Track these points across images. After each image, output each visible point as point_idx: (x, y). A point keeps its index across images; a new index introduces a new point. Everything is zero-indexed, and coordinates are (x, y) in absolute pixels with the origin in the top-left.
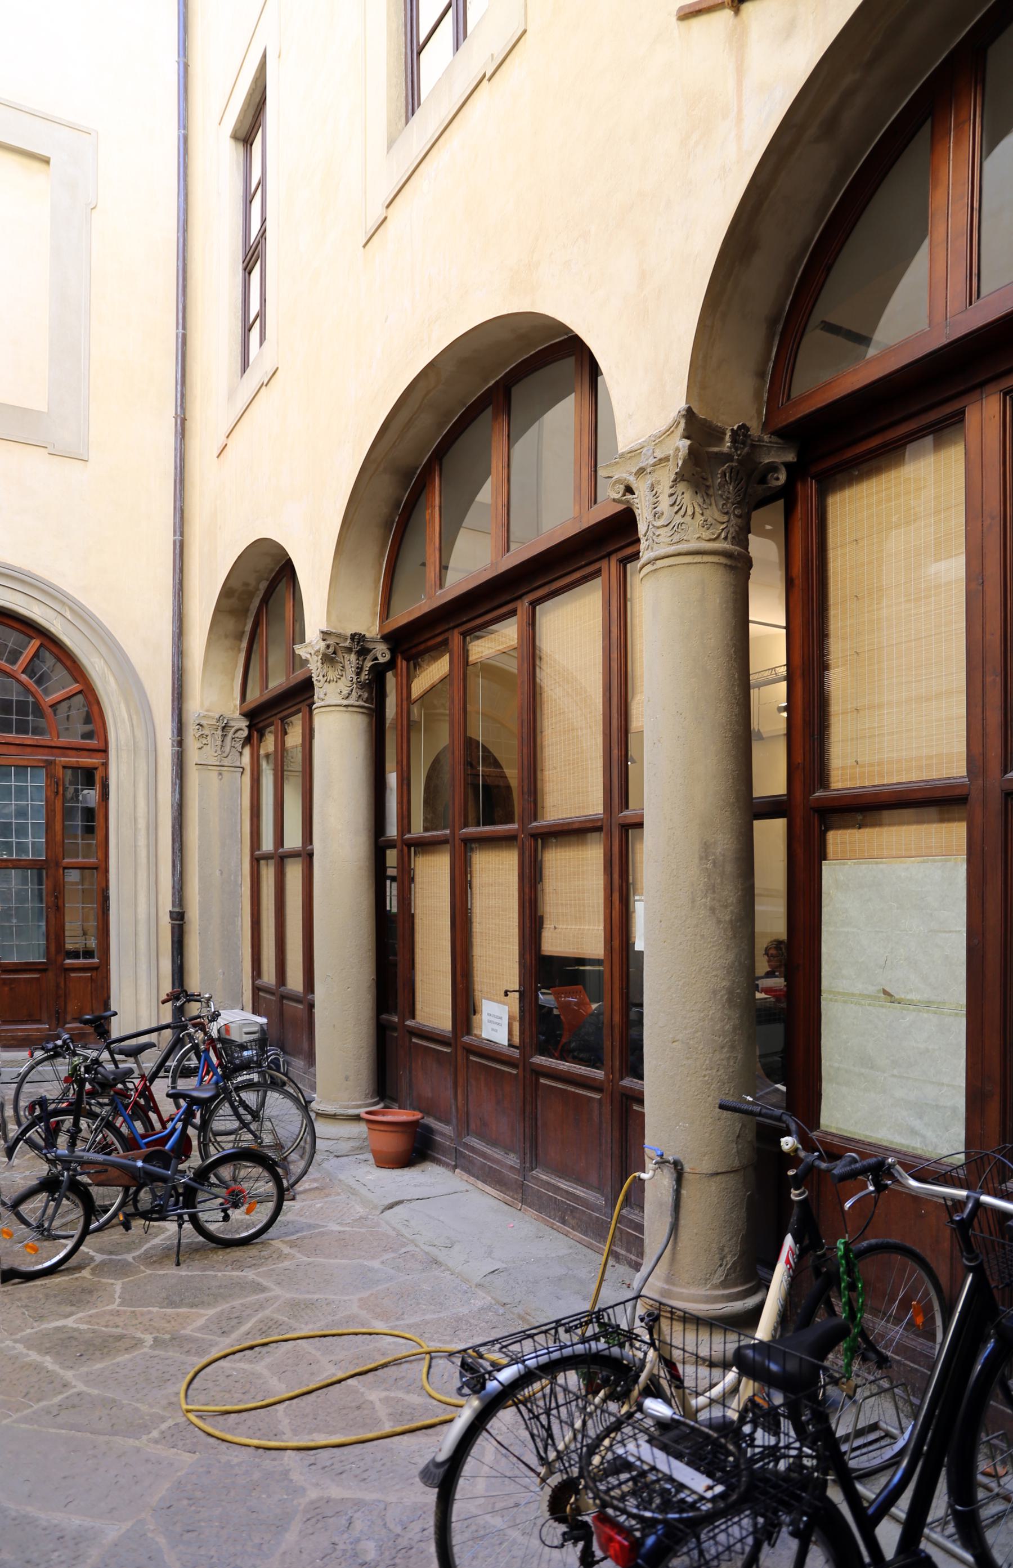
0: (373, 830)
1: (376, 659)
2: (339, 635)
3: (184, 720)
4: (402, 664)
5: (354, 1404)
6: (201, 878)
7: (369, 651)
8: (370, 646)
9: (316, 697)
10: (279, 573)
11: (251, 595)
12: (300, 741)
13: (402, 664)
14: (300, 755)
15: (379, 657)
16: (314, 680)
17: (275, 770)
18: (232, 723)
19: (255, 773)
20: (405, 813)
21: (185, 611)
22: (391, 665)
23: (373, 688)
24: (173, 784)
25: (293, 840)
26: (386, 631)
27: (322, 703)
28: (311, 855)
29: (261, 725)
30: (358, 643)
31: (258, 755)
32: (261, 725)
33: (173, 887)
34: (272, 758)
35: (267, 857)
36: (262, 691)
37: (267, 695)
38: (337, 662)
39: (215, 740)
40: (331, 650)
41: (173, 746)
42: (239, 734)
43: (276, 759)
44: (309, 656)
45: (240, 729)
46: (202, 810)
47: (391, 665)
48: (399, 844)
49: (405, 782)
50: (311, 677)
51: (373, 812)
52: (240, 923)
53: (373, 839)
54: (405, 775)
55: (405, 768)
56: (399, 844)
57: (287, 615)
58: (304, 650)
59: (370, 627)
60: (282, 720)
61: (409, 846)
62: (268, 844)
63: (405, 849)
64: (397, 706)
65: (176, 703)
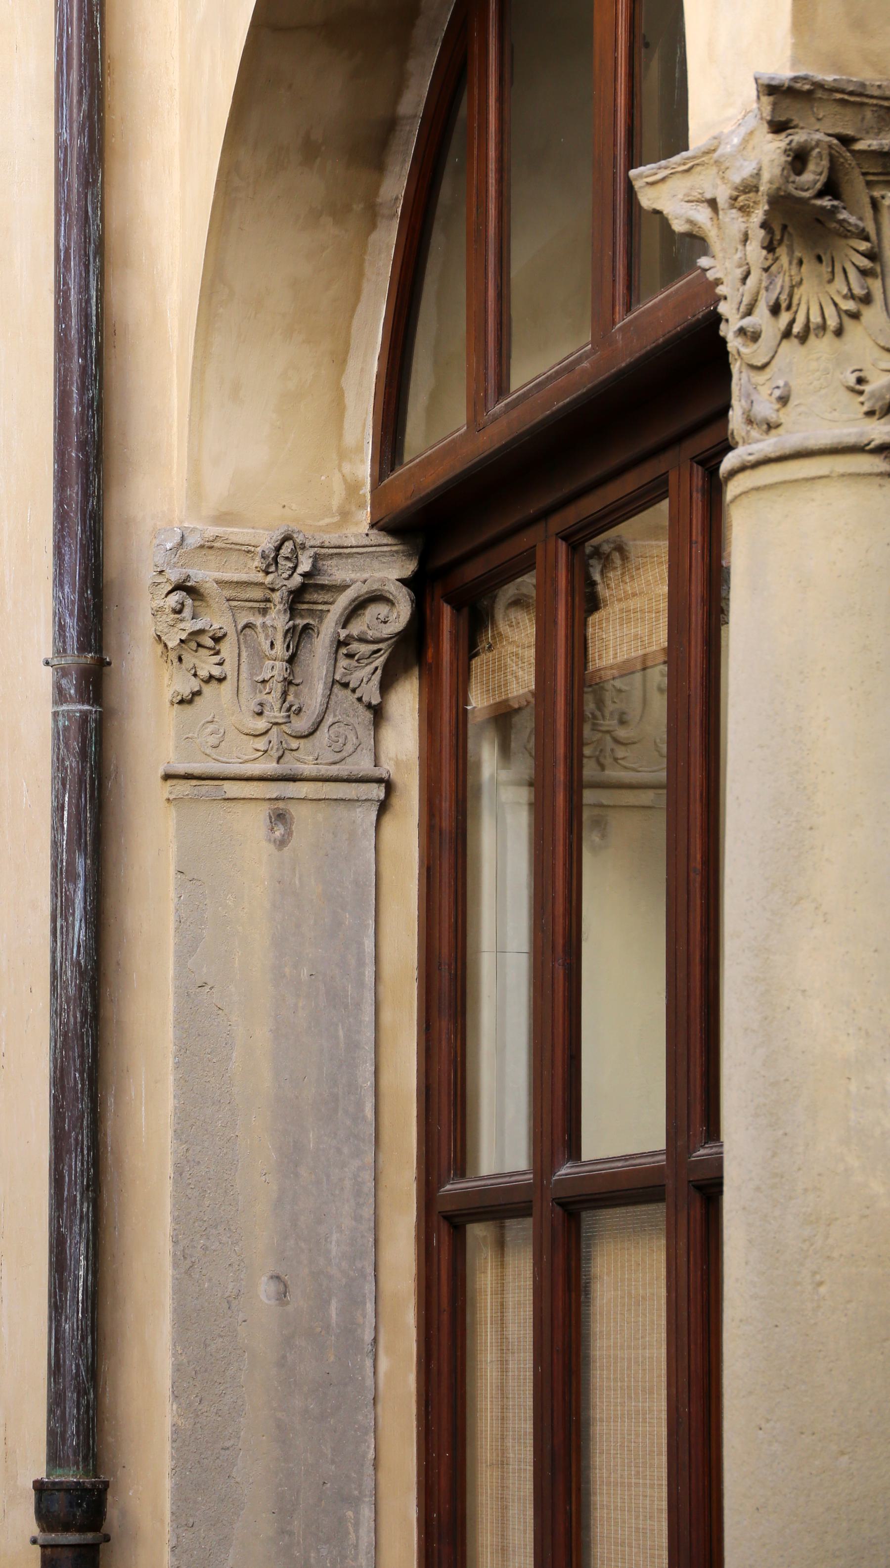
2: (851, 98)
3: (112, 571)
5: (270, 586)
6: (183, 1320)
9: (736, 417)
12: (661, 638)
14: (659, 705)
16: (728, 331)
17: (539, 785)
21: (115, 45)
24: (62, 876)
25: (624, 1119)
27: (767, 445)
28: (709, 1191)
29: (473, 571)
31: (461, 717)
32: (473, 571)
33: (56, 1370)
34: (525, 725)
35: (501, 1206)
37: (503, 425)
38: (846, 232)
39: (259, 657)
40: (813, 175)
41: (60, 696)
42: (368, 623)
43: (543, 732)
44: (702, 215)
45: (376, 598)
46: (192, 993)
50: (716, 319)
52: (366, 1537)
58: (680, 186)
60: (575, 539)
62: (503, 1144)
65: (74, 492)
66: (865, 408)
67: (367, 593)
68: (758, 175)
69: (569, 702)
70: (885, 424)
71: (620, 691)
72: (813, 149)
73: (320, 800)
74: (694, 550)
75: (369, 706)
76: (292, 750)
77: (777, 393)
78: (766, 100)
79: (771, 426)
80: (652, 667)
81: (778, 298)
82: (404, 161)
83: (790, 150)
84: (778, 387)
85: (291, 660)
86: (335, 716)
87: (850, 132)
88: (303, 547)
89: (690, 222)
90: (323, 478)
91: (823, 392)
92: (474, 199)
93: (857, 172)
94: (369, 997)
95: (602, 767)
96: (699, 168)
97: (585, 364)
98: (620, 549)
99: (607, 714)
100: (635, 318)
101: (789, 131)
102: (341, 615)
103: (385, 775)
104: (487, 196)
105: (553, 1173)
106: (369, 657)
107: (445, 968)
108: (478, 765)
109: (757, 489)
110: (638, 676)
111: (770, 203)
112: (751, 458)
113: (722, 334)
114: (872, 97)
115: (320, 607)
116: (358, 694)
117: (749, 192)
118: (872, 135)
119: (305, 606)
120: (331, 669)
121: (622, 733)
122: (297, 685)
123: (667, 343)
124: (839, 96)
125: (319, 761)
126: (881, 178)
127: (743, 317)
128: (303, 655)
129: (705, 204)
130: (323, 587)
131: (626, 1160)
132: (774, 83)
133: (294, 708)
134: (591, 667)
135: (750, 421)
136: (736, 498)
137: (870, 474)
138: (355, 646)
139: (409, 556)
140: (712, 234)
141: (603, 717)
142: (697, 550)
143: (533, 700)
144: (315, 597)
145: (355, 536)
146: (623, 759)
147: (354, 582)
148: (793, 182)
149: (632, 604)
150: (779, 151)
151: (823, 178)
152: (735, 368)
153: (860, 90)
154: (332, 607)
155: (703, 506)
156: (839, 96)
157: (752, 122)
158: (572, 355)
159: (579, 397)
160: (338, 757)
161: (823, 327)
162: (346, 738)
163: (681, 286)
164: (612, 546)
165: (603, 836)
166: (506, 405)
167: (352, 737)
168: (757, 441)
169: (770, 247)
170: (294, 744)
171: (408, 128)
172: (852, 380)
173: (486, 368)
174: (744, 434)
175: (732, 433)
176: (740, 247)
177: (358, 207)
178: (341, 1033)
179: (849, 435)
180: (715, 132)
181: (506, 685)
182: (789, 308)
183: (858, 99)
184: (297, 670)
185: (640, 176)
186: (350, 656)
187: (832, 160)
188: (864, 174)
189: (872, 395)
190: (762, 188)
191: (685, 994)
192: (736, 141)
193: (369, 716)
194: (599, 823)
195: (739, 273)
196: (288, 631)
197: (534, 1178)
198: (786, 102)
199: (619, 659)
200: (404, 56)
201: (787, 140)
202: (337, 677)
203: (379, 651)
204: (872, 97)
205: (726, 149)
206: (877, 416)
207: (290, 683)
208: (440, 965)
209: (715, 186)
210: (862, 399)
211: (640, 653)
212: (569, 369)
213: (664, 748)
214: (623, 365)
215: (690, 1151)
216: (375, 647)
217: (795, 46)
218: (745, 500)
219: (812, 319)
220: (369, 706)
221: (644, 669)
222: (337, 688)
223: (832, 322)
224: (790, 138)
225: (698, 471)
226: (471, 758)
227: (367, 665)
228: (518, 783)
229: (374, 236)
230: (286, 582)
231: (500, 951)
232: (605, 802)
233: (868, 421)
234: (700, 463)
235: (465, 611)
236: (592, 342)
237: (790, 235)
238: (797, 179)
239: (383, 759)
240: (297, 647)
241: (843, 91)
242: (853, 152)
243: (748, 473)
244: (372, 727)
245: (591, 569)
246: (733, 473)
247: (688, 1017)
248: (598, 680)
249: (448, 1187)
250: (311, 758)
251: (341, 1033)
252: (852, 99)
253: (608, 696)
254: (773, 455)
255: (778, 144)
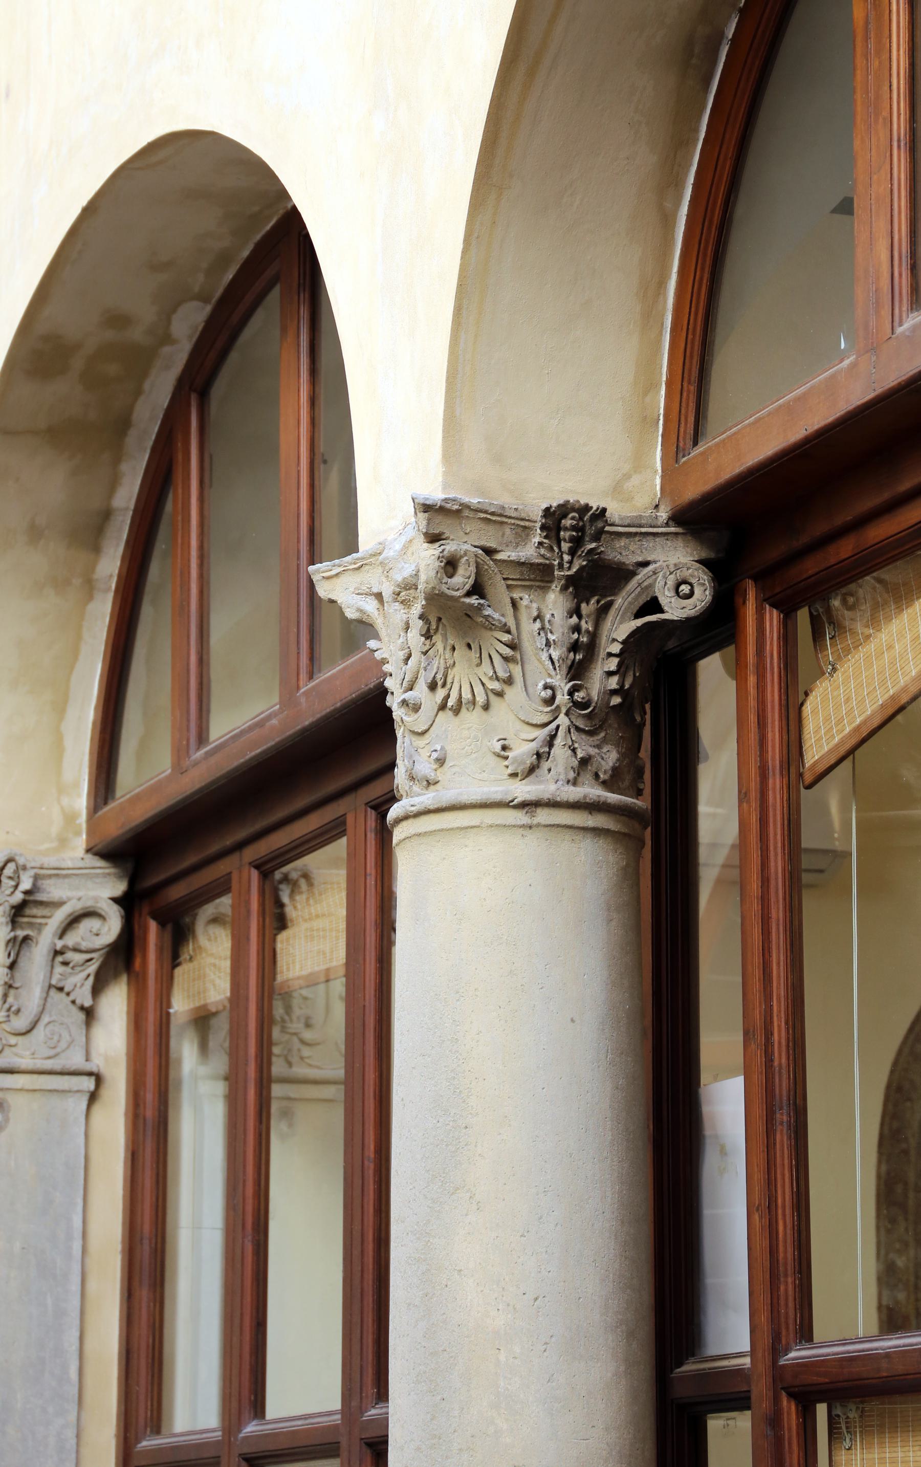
0: (646, 1330)
1: (653, 606)
2: (493, 517)
4: (759, 621)
7: (621, 575)
8: (625, 553)
9: (400, 773)
10: (251, 270)
11: (138, 362)
12: (340, 955)
13: (759, 621)
14: (339, 1010)
15: (666, 598)
16: (393, 702)
17: (233, 1081)
18: (53, 890)
19: (150, 1097)
20: (787, 1252)
22: (717, 627)
23: (643, 727)
26: (693, 490)
27: (427, 799)
29: (177, 892)
30: (577, 543)
32: (177, 892)
36: (180, 752)
38: (490, 626)
40: (463, 578)
44: (370, 606)
45: (89, 914)
47: (717, 627)
48: (760, 1390)
49: (782, 1116)
50: (382, 692)
51: (647, 1229)
53: (645, 1371)
54: (782, 1085)
55: (780, 1058)
56: (760, 1390)
57: (286, 439)
59: (618, 468)
60: (266, 868)
61: (806, 1400)
63: (790, 1409)
64: (743, 796)
66: (509, 771)
67: (82, 909)
68: (417, 575)
69: (260, 1009)
70: (526, 785)
71: (306, 999)
72: (461, 557)
73: (35, 1091)
74: (368, 881)
75: (82, 1008)
76: (11, 1046)
77: (435, 755)
78: (421, 515)
79: (429, 783)
80: (336, 979)
81: (434, 677)
82: (118, 545)
83: (443, 557)
84: (436, 751)
85: (12, 966)
86: (51, 1016)
87: (492, 544)
88: (24, 868)
89: (360, 610)
90: (43, 809)
91: (474, 756)
92: (178, 579)
93: (499, 577)
94: (76, 1268)
95: (290, 1064)
96: (367, 567)
97: (274, 722)
98: (306, 876)
99: (294, 1018)
100: (317, 685)
101: (441, 542)
102: (58, 927)
103: (95, 1070)
104: (189, 578)
105: (240, 1431)
106: (83, 965)
107: (146, 1242)
108: (179, 1062)
109: (419, 835)
110: (322, 987)
111: (426, 599)
112: (413, 809)
113: (388, 704)
114: (510, 517)
115: (39, 921)
116: (72, 997)
117: (409, 589)
118: (511, 548)
119: (25, 920)
120: (48, 975)
121: (308, 1035)
122: (17, 988)
123: (345, 706)
124: (483, 515)
125: (35, 1056)
126: (519, 583)
127: (405, 692)
128: (22, 963)
129: (373, 597)
130: (41, 903)
131: (306, 1419)
132: (428, 503)
133: (13, 1009)
134: (279, 978)
135: (412, 778)
136: (400, 842)
137: (514, 826)
138: (70, 956)
139: (120, 877)
140: (379, 623)
141: (291, 1021)
142: (371, 881)
143: (228, 1005)
144: (34, 911)
145: (72, 859)
146: (309, 1057)
147: (69, 899)
148: (446, 583)
149: (316, 924)
150: (433, 557)
151: (471, 581)
152: (399, 733)
153: (500, 511)
154: (50, 921)
155: (376, 844)
156: (483, 515)
157: (411, 532)
158: (262, 713)
159: (269, 749)
160: (52, 1052)
161: (474, 702)
162: (60, 1036)
163: (356, 661)
164: (299, 873)
165: (290, 1125)
166: (206, 753)
167: (65, 1034)
168: (419, 795)
169: (428, 635)
170: (13, 1040)
171: (121, 518)
172: (498, 747)
173: (188, 721)
174: (407, 788)
175: (397, 787)
176: (402, 634)
177: (77, 581)
178: (49, 1301)
179: (496, 792)
180: (381, 539)
181: (204, 992)
182: (444, 685)
183: (499, 519)
184: (17, 975)
185: (318, 571)
186: (65, 964)
187: (478, 566)
188: (505, 579)
189: (515, 759)
190: (419, 587)
191: (360, 1268)
192: (398, 547)
193: (82, 1016)
194: (286, 1114)
195: (402, 655)
196: (9, 941)
197: (223, 1436)
198: (439, 518)
199: (304, 973)
200: (117, 460)
201: (440, 549)
202: (54, 982)
203: (90, 960)
204: (510, 517)
205: (389, 553)
206: (519, 778)
207: (10, 986)
208: (142, 1239)
209: (381, 583)
210: (506, 763)
211: (323, 967)
212: (260, 724)
213: (343, 1047)
214: (307, 723)
215: (362, 1411)
216: (88, 956)
217: (445, 474)
218: (407, 844)
219: (463, 695)
220: (82, 1008)
221: (327, 981)
222: (53, 992)
223: (481, 699)
224: (442, 547)
225: (372, 815)
226: (173, 1055)
227: (81, 971)
228: (215, 1078)
229: (91, 606)
230: (8, 898)
231: (197, 1227)
232: (292, 1095)
233: (511, 781)
234: (373, 808)
235: (169, 927)
236: (281, 703)
237: (444, 626)
238: (449, 580)
239: (94, 1054)
240: (18, 955)
241: (486, 512)
242: (495, 561)
243: (410, 821)
244: (84, 1027)
245: (281, 893)
246: (398, 821)
247: (362, 1289)
248: (287, 990)
249: (144, 1443)
250: (28, 1053)
251: (49, 1301)
252: (494, 518)
253: (296, 1002)
254: (432, 807)
255: (431, 552)
